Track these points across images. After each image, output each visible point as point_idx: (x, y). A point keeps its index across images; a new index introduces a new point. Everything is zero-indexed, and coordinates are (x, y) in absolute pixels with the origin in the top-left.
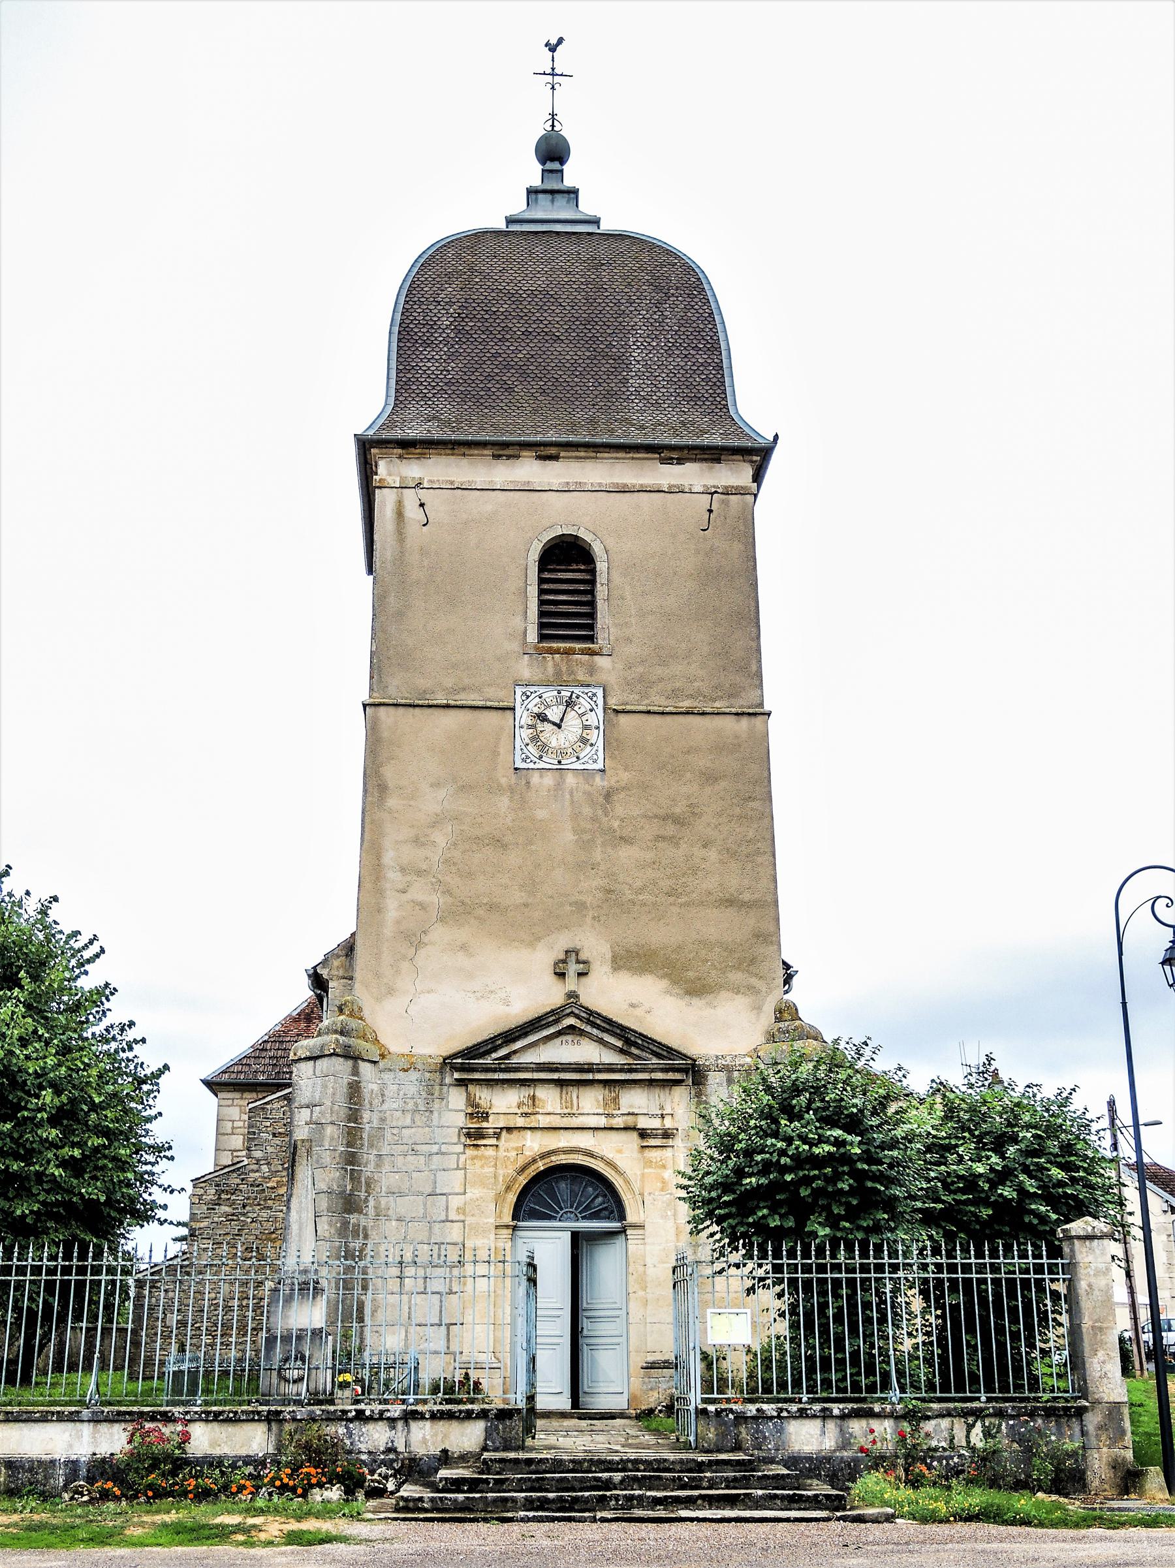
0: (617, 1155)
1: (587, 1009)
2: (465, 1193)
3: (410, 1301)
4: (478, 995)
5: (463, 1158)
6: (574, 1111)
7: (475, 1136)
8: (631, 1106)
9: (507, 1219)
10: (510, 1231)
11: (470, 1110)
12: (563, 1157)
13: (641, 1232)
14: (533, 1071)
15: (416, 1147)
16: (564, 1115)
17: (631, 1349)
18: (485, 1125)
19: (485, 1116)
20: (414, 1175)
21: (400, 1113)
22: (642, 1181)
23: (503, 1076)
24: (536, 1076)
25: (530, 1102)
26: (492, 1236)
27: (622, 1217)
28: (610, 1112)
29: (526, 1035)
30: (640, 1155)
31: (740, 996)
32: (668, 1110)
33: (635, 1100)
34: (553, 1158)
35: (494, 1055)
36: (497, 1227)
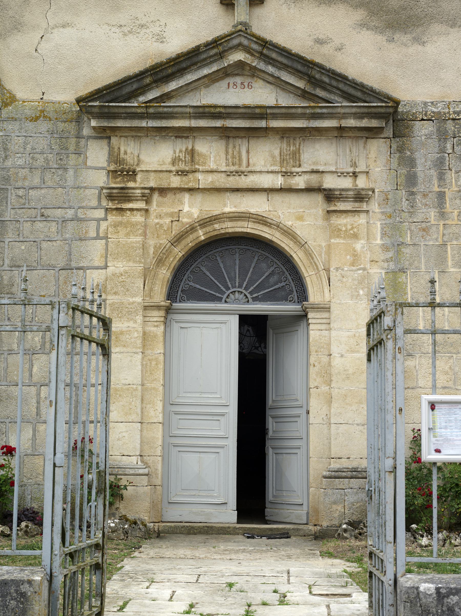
0: (297, 223)
1: (258, 38)
2: (106, 267)
3: (38, 394)
4: (126, 29)
5: (104, 225)
6: (243, 168)
7: (118, 198)
8: (315, 163)
9: (159, 296)
10: (162, 313)
11: (112, 168)
12: (230, 224)
13: (325, 315)
14: (190, 117)
15: (47, 212)
16: (229, 174)
17: (311, 455)
18: (131, 184)
19: (131, 174)
20: (45, 245)
21: (27, 170)
22: (328, 253)
23: (152, 123)
24: (194, 123)
25: (188, 158)
26: (139, 319)
27: (303, 295)
28: (289, 169)
29: (181, 72)
30: (325, 223)
31: (456, 29)
32: (362, 167)
33: (322, 156)
34: (217, 226)
35: (142, 99)
36: (146, 308)
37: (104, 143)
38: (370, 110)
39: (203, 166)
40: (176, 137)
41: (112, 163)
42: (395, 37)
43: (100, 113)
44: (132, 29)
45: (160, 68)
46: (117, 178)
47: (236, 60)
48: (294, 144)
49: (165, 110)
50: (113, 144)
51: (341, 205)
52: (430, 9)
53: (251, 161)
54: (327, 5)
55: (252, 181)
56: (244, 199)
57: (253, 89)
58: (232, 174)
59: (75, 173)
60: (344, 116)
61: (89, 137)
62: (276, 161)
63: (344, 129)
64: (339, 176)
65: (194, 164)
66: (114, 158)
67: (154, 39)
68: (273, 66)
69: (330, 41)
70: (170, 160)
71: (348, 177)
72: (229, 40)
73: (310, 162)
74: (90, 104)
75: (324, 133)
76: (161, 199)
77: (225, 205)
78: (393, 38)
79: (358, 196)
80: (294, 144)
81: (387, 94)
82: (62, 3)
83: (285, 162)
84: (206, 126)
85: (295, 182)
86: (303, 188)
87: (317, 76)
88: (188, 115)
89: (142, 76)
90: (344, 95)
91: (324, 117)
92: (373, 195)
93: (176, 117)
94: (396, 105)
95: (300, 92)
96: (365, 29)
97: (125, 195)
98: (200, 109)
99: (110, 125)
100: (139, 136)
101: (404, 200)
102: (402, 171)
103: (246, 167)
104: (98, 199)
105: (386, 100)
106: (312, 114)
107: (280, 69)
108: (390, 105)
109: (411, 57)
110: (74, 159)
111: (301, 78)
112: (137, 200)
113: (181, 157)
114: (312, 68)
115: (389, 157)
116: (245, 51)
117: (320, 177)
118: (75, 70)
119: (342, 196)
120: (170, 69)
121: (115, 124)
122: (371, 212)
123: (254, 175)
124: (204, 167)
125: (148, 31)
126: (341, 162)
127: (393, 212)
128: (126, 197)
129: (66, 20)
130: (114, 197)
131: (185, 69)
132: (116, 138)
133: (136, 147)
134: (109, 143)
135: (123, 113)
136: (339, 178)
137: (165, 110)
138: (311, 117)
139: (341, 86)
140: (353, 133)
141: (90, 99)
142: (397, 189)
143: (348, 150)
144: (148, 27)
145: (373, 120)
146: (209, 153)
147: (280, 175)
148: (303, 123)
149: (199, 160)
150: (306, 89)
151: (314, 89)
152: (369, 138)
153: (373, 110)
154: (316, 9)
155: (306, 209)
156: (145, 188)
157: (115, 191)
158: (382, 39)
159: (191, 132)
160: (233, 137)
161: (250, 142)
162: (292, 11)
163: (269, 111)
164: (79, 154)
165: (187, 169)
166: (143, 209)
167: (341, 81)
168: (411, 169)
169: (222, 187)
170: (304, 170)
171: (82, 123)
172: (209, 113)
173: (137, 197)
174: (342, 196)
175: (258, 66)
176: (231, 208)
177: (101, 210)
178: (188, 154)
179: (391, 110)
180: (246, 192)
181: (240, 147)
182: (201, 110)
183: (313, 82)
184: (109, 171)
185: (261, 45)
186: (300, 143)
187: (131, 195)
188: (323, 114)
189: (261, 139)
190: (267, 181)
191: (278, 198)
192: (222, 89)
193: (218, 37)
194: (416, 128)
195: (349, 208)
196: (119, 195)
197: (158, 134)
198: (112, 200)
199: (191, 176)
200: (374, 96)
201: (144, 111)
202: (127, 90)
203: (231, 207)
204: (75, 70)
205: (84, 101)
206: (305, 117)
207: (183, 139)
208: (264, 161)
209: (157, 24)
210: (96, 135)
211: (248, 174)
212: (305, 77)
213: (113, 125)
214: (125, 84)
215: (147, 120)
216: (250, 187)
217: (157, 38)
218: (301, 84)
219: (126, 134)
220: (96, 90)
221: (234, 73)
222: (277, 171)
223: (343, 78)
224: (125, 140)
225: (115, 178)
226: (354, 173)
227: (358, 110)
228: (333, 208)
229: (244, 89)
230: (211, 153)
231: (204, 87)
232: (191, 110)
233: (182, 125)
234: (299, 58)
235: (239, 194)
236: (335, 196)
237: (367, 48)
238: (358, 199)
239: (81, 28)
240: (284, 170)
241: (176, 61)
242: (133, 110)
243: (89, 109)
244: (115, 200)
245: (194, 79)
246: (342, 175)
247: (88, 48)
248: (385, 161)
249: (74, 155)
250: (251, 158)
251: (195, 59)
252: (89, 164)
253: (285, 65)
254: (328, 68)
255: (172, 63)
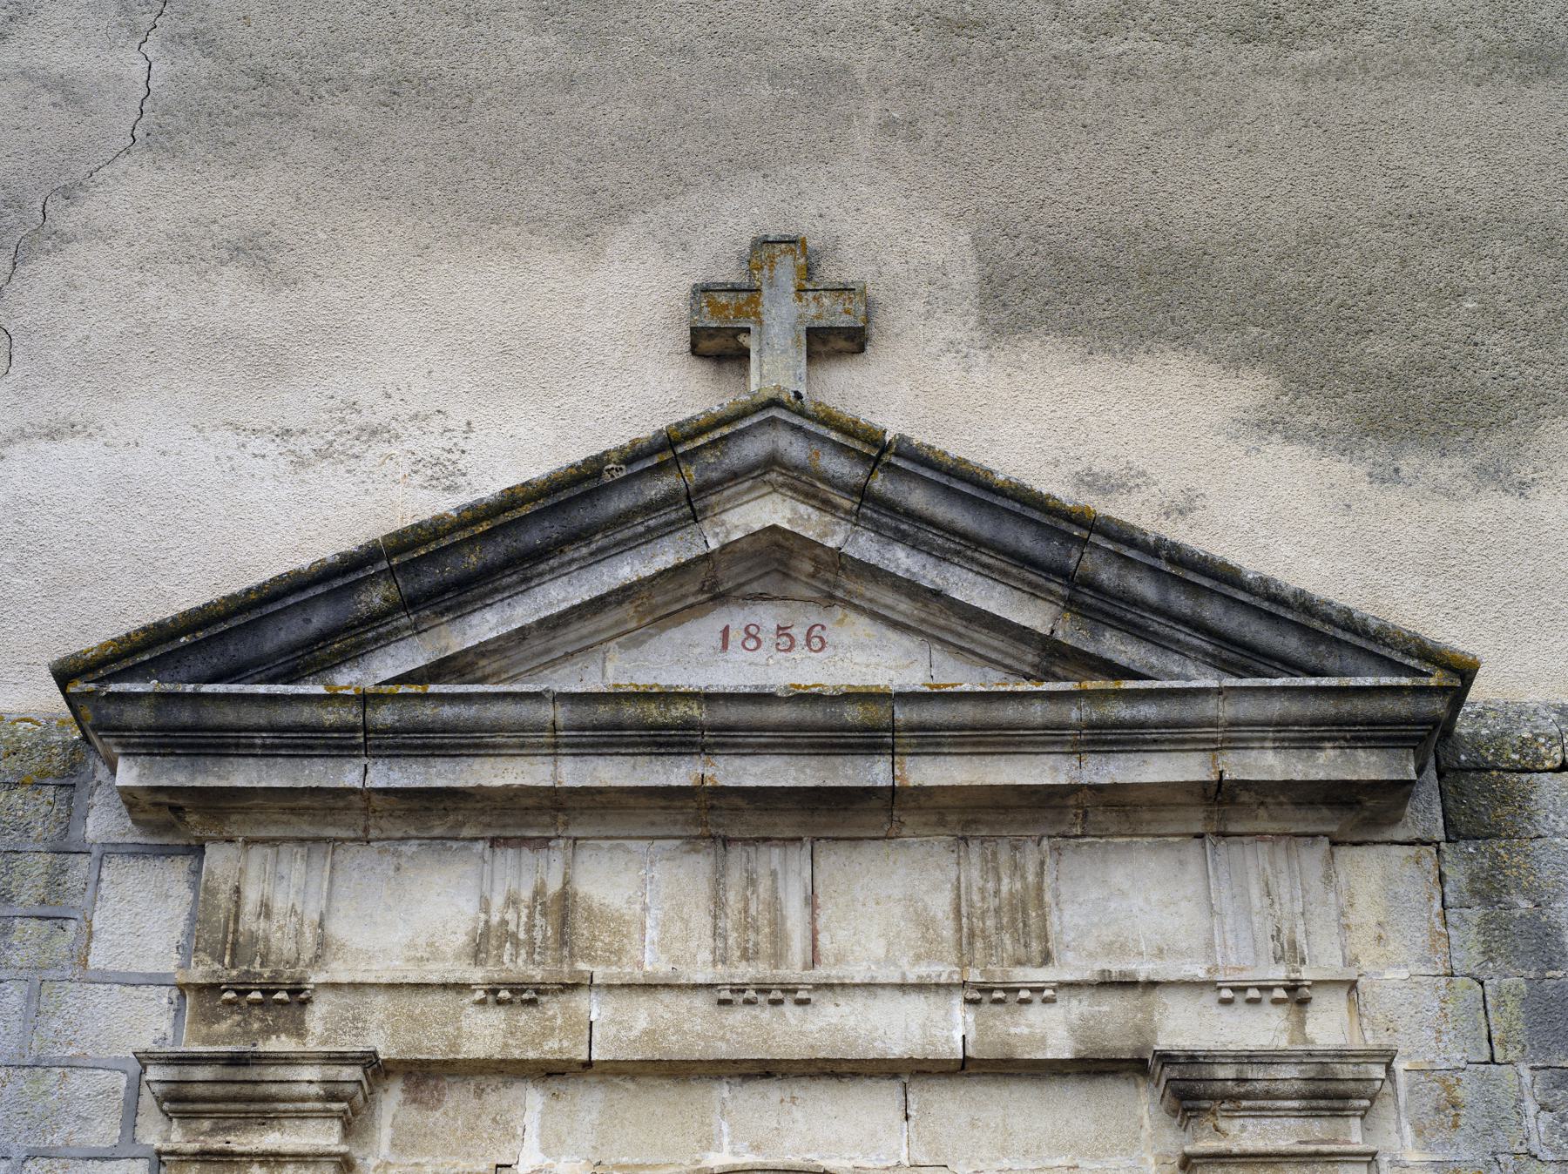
1: (851, 429)
6: (794, 969)
11: (198, 974)
14: (558, 743)
16: (729, 996)
24: (573, 773)
25: (544, 929)
28: (998, 974)
29: (525, 567)
32: (1323, 961)
35: (347, 679)
37: (174, 873)
38: (1346, 707)
39: (608, 962)
40: (494, 842)
41: (202, 955)
42: (1401, 464)
43: (157, 729)
44: (331, 444)
45: (433, 546)
46: (219, 1019)
47: (757, 527)
48: (1016, 868)
49: (447, 712)
50: (211, 873)
51: (1243, 1128)
52: (1530, 370)
53: (824, 939)
54: (1119, 356)
55: (835, 1030)
56: (797, 1114)
57: (828, 651)
58: (740, 998)
59: (28, 999)
60: (1236, 735)
61: (110, 850)
62: (940, 940)
63: (1233, 800)
64: (1226, 1002)
65: (572, 955)
66: (211, 932)
67: (417, 480)
68: (915, 546)
69: (1138, 481)
70: (461, 939)
71: (1267, 1008)
72: (725, 438)
73: (1090, 944)
74: (114, 688)
75: (1147, 816)
76: (413, 1115)
77: (709, 1143)
78: (1397, 470)
79: (1323, 1086)
80: (1016, 868)
81: (1416, 637)
82: (56, 353)
83: (979, 944)
84: (627, 784)
85: (1026, 1031)
86: (1067, 1055)
87: (1104, 576)
88: (546, 738)
89: (352, 578)
90: (1225, 654)
91: (1146, 742)
92: (1388, 1088)
93: (495, 746)
94: (1459, 683)
95: (1029, 658)
96: (1276, 437)
97: (248, 1090)
98: (601, 708)
99: (197, 784)
100: (327, 840)
101: (1531, 1107)
102: (1507, 981)
103: (805, 969)
104: (125, 1114)
105: (1413, 663)
106: (1091, 726)
107: (943, 557)
108: (1432, 682)
109: (1478, 536)
110: (34, 939)
111: (1035, 592)
112: (302, 1116)
113: (512, 927)
114: (1084, 542)
115: (1438, 922)
116: (795, 490)
117: (1140, 1009)
118: (83, 594)
119: (1248, 1087)
120: (472, 551)
121: (220, 777)
122: (1384, 1161)
123: (841, 1001)
124: (615, 969)
125: (395, 449)
126: (1230, 943)
127: (1487, 1163)
128: (251, 1100)
129: (63, 411)
130: (195, 1100)
131: (538, 555)
132: (230, 851)
133: (313, 888)
134: (197, 872)
135: (260, 729)
136: (1225, 1011)
137: (447, 712)
138: (1089, 742)
139: (1212, 612)
140: (1272, 818)
141: (116, 667)
142: (1493, 1061)
143: (1255, 892)
144: (397, 437)
145: (1361, 754)
146: (638, 907)
147: (957, 1001)
148: (1055, 769)
149: (594, 938)
150: (1059, 635)
151: (1094, 637)
152: (1343, 843)
153: (1362, 707)
154: (1074, 370)
155: (1083, 1155)
156: (341, 1059)
157: (200, 1073)
158: (1351, 471)
159: (561, 817)
160: (745, 841)
161: (821, 861)
162: (978, 377)
163: (903, 715)
164: (60, 920)
165: (538, 975)
166: (329, 1155)
167: (1212, 592)
168: (1542, 971)
169: (697, 1056)
170: (1068, 978)
171: (86, 791)
172: (640, 726)
173: (303, 1099)
174: (1248, 1087)
175: (847, 550)
176: (734, 1153)
177: (133, 1164)
178: (544, 914)
179: (1438, 706)
180: (804, 1082)
181: (774, 881)
182: (604, 712)
183: (1089, 607)
184: (183, 988)
185: (864, 458)
186: (1042, 863)
187: (274, 1089)
188: (1142, 725)
189: (869, 849)
190: (899, 1027)
191: (950, 1106)
192: (697, 651)
193: (679, 425)
194: (1543, 802)
195: (1284, 1144)
196: (219, 1090)
197: (413, 833)
198: (186, 1117)
199: (553, 1007)
200: (1360, 649)
201: (351, 718)
202: (283, 634)
203: (738, 1147)
204: (83, 594)
205: (91, 676)
206: (1063, 743)
207: (526, 851)
208: (882, 942)
209: (436, 423)
210: (141, 840)
211: (813, 997)
212: (1053, 586)
213: (213, 782)
214: (278, 606)
215: (366, 761)
216: (822, 1055)
217: (429, 472)
218: (1035, 616)
219: (274, 832)
220: (144, 629)
221: (748, 589)
222: (943, 980)
223: (1219, 578)
224: (265, 857)
225: (211, 1017)
226: (1293, 987)
227: (1294, 708)
228: (1208, 1145)
229: (789, 650)
230: (645, 909)
231: (620, 646)
232: (561, 714)
233: (519, 781)
234: (1024, 503)
235: (773, 1092)
236: (1218, 1087)
237: (1294, 504)
238: (1322, 1103)
239: (122, 441)
240: (974, 976)
241: (502, 519)
242: (306, 714)
243: (111, 710)
244: (198, 1116)
245: (577, 602)
246: (1239, 998)
247: (143, 510)
248: (1421, 939)
249: (34, 923)
250: (827, 928)
251: (583, 516)
252: (97, 960)
253: (964, 535)
254: (1151, 540)
255: (485, 526)
